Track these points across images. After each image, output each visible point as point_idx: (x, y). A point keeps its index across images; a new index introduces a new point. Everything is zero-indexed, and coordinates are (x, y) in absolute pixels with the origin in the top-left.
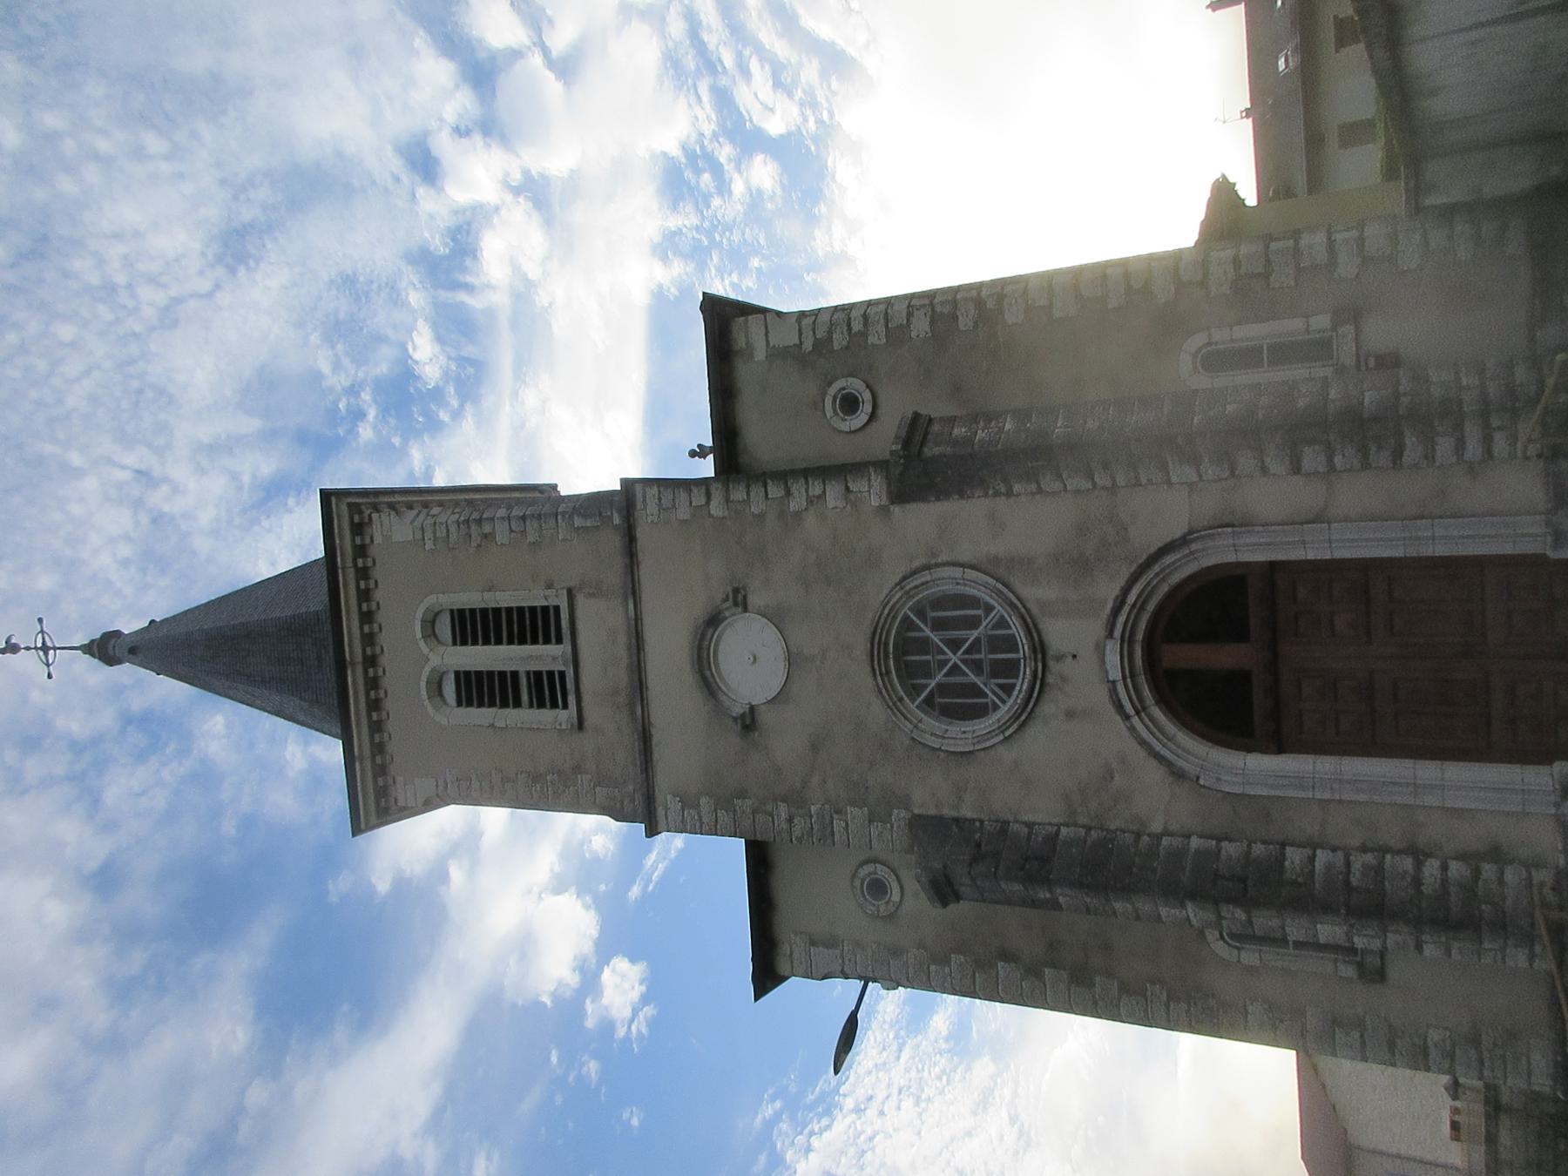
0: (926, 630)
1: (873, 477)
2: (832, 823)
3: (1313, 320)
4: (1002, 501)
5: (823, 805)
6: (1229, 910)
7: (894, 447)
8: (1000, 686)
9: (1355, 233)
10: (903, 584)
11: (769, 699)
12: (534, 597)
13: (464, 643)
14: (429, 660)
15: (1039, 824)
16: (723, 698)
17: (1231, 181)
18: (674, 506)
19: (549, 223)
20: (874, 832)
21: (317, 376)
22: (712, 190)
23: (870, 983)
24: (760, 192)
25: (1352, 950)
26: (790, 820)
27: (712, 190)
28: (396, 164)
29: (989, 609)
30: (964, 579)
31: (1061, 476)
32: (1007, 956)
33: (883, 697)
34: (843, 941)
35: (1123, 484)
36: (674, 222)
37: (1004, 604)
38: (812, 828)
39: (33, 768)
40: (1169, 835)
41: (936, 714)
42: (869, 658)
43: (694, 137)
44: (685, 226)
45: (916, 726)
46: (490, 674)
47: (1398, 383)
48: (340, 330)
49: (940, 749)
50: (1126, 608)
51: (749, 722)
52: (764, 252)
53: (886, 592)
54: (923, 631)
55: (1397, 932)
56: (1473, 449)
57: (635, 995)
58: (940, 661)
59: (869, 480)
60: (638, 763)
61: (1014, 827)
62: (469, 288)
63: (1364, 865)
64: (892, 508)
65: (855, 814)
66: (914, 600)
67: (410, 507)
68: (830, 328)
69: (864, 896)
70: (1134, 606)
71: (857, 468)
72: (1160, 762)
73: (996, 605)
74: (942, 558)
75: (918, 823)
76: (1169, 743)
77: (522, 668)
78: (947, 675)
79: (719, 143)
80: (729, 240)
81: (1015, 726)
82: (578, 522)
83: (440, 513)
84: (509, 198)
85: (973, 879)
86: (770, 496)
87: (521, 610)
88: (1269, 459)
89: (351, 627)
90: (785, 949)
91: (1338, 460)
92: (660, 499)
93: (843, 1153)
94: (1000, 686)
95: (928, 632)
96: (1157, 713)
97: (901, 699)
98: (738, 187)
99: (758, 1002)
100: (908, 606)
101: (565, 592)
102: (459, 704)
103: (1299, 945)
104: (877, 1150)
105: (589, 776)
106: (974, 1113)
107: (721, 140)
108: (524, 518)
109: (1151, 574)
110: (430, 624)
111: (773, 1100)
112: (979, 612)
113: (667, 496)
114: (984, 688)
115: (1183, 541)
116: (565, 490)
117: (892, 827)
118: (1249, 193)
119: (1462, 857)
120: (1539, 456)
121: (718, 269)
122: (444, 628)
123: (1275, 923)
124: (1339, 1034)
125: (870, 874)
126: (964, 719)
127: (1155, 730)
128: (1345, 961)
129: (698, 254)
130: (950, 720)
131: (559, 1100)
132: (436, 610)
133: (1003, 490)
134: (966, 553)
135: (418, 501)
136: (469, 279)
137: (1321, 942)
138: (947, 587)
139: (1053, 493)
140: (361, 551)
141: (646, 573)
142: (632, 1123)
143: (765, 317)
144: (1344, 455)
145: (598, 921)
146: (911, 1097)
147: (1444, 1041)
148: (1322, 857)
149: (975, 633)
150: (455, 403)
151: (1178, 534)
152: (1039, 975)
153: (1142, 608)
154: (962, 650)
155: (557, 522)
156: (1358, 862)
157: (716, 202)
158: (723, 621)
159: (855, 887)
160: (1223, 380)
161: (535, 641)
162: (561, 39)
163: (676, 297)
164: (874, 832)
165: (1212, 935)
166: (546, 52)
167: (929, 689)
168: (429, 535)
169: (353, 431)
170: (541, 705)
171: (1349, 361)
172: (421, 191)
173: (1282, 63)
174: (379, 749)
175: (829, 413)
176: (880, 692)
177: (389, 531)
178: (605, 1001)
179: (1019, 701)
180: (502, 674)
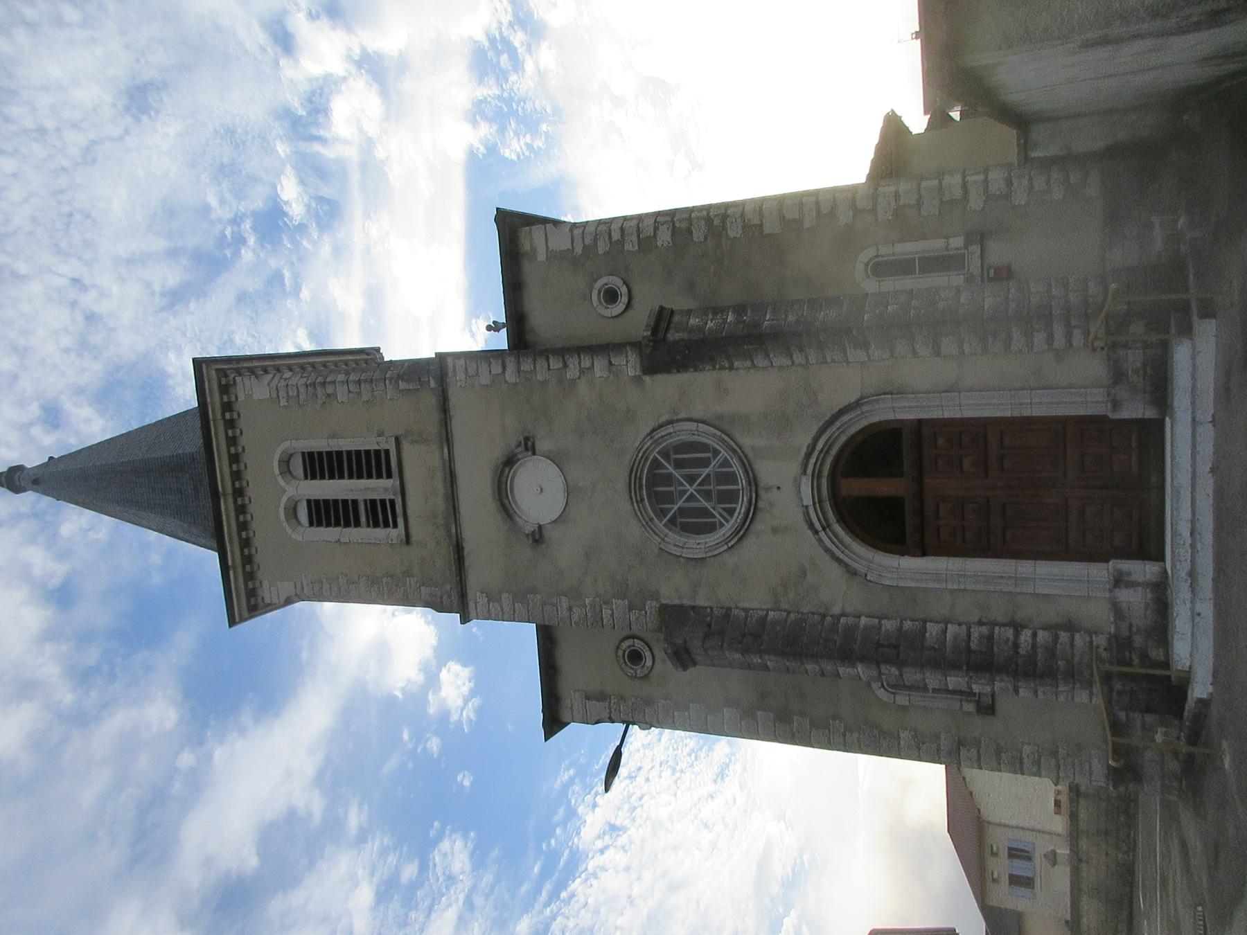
0: (669, 467)
1: (629, 354)
3: (951, 240)
4: (725, 373)
5: (594, 598)
8: (724, 509)
11: (553, 520)
12: (369, 443)
13: (314, 477)
14: (286, 491)
15: (753, 610)
16: (518, 519)
17: (899, 114)
18: (477, 374)
20: (633, 618)
21: (207, 208)
22: (510, 68)
27: (510, 68)
28: (262, 37)
29: (716, 452)
31: (768, 356)
36: (481, 92)
40: (845, 616)
41: (678, 529)
43: (494, 25)
44: (490, 96)
45: (663, 540)
49: (681, 556)
50: (816, 454)
51: (538, 537)
52: (550, 118)
54: (668, 469)
55: (1002, 680)
56: (1059, 341)
57: (465, 690)
58: (680, 491)
59: (627, 356)
60: (454, 568)
61: (735, 612)
62: (322, 140)
64: (644, 377)
65: (619, 605)
69: (625, 663)
70: (821, 451)
73: (722, 450)
74: (683, 415)
75: (664, 610)
76: (846, 550)
78: (687, 501)
79: (514, 30)
80: (523, 108)
81: (736, 539)
82: (402, 385)
84: (353, 69)
86: (551, 368)
91: (966, 347)
93: (619, 809)
94: (724, 509)
96: (838, 528)
97: (651, 520)
98: (529, 66)
99: (547, 742)
100: (657, 451)
102: (311, 524)
104: (645, 807)
106: (715, 781)
109: (834, 428)
110: (286, 463)
111: (568, 769)
112: (710, 455)
115: (857, 404)
117: (646, 613)
118: (917, 122)
119: (1046, 628)
122: (297, 466)
123: (919, 677)
125: (629, 647)
131: (411, 766)
132: (292, 506)
134: (698, 411)
135: (271, 366)
136: (322, 133)
137: (950, 688)
139: (765, 368)
140: (228, 407)
145: (436, 634)
146: (669, 769)
149: (707, 471)
151: (853, 399)
153: (827, 452)
154: (696, 484)
155: (385, 385)
156: (976, 632)
157: (513, 78)
158: (517, 462)
159: (619, 656)
161: (370, 476)
163: (483, 155)
165: (875, 686)
168: (282, 394)
169: (237, 253)
170: (376, 525)
171: (976, 271)
172: (283, 62)
174: (248, 560)
175: (595, 303)
177: (252, 392)
178: (443, 693)
180: (345, 502)
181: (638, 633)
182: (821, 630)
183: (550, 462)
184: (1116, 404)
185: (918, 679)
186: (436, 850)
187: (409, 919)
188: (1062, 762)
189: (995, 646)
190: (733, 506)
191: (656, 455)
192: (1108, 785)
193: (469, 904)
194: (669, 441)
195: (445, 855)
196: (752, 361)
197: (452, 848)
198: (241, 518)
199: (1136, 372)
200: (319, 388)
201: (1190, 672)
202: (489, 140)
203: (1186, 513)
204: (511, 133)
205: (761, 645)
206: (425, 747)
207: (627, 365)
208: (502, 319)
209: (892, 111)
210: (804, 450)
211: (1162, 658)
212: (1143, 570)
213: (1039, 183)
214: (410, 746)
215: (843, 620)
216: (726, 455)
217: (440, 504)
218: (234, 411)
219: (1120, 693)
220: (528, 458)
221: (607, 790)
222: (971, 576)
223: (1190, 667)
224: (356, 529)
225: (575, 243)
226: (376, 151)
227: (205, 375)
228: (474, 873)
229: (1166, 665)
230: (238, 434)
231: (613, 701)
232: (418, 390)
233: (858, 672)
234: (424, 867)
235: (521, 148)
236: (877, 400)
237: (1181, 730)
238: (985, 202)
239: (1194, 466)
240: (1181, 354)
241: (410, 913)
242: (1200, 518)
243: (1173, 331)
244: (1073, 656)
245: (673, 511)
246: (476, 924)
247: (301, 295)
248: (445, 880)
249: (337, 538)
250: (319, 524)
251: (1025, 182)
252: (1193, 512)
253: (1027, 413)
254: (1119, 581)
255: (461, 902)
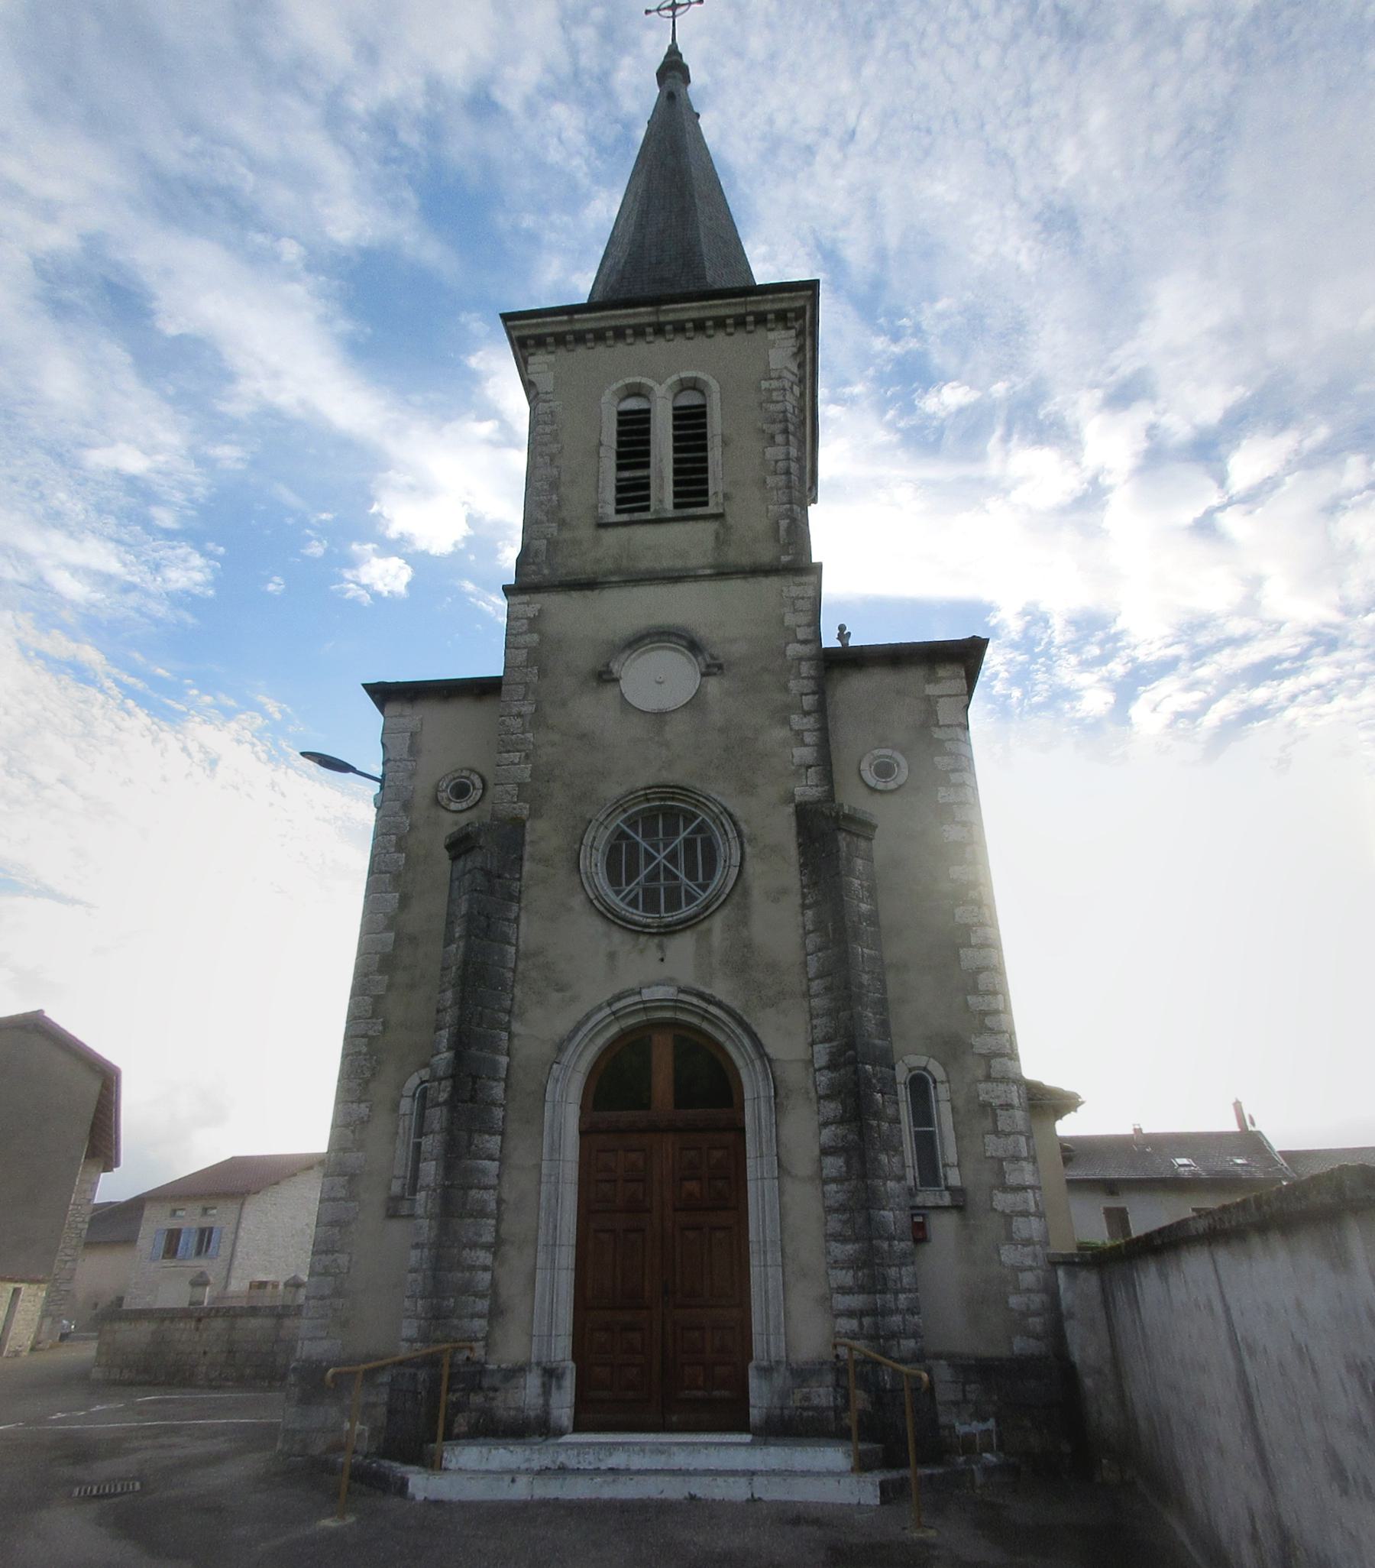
1: (819, 789)
2: (518, 751)
3: (956, 1171)
4: (798, 900)
6: (446, 1087)
7: (846, 808)
8: (637, 895)
9: (1033, 1209)
10: (725, 814)
11: (626, 695)
12: (716, 484)
13: (676, 417)
14: (660, 385)
15: (518, 928)
16: (626, 655)
17: (1079, 1109)
19: (1063, 511)
20: (509, 787)
21: (933, 298)
22: (1084, 657)
23: (379, 784)
24: (1079, 698)
25: (414, 1190)
26: (519, 715)
28: (1126, 370)
30: (729, 867)
31: (820, 950)
32: (404, 901)
33: (627, 796)
34: (415, 761)
35: (813, 1004)
36: (1057, 623)
37: (707, 901)
38: (513, 734)
39: (586, 35)
40: (509, 1038)
41: (613, 841)
42: (660, 784)
43: (1133, 640)
45: (602, 823)
46: (647, 442)
47: (901, 1240)
48: (974, 322)
49: (581, 843)
50: (704, 1005)
51: (605, 677)
52: (1026, 701)
53: (719, 799)
54: (684, 830)
55: (430, 1228)
56: (843, 1302)
57: (380, 586)
58: (658, 845)
59: (817, 786)
60: (568, 578)
61: (515, 908)
62: (1006, 439)
63: (485, 1201)
64: (793, 805)
65: (525, 772)
66: (711, 824)
67: (801, 366)
68: (952, 754)
69: (454, 779)
70: (706, 1011)
71: (828, 776)
72: (571, 1032)
73: (707, 894)
74: (748, 849)
75: (517, 826)
77: (652, 472)
79: (1127, 662)
80: (1038, 670)
81: (602, 909)
82: (784, 523)
83: (794, 395)
84: (1088, 474)
85: (470, 871)
86: (804, 697)
87: (705, 470)
88: (833, 1129)
89: (691, 311)
90: (407, 710)
91: (833, 1187)
92: (803, 598)
94: (637, 895)
95: (683, 835)
96: (614, 1029)
97: (625, 811)
98: (1086, 679)
101: (721, 511)
102: (620, 413)
103: (418, 1147)
105: (555, 534)
107: (1130, 665)
108: (788, 472)
109: (733, 1025)
112: (701, 880)
113: (805, 605)
114: (635, 882)
115: (763, 1054)
116: (812, 510)
117: (515, 803)
118: (1067, 1127)
119: (494, 1284)
120: (837, 1356)
121: (1011, 661)
122: (689, 399)
123: (436, 1126)
124: (343, 1180)
125: (473, 785)
126: (608, 863)
127: (600, 1027)
128: (404, 1185)
129: (1027, 643)
130: (607, 853)
133: (807, 901)
134: (753, 868)
136: (1015, 437)
137: (421, 1165)
138: (722, 850)
139: (804, 945)
140: (761, 319)
141: (736, 585)
142: (271, 585)
143: (964, 695)
144: (837, 1192)
147: (338, 1267)
148: (492, 1166)
149: (682, 876)
150: (902, 424)
151: (769, 1050)
152: (388, 928)
153: (704, 1018)
156: (490, 1196)
157: (1073, 659)
160: (903, 1093)
161: (676, 483)
162: (1231, 521)
163: (988, 622)
164: (509, 787)
165: (425, 1073)
166: (1221, 508)
167: (632, 834)
168: (775, 384)
169: (880, 331)
170: (619, 489)
171: (919, 1200)
172: (1099, 394)
173: (1184, 1161)
174: (580, 338)
176: (632, 793)
177: (779, 344)
178: (374, 560)
179: (623, 912)
180: (647, 453)
181: (489, 794)
182: (493, 1009)
183: (693, 693)
184: (766, 1372)
185: (433, 1126)
186: (190, 550)
187: (105, 515)
188: (328, 1302)
189: (472, 1220)
190: (641, 906)
191: (701, 818)
192: (297, 1360)
193: (128, 588)
194: (717, 833)
195: (185, 560)
196: (812, 932)
197: (193, 568)
198: (629, 332)
199: (807, 1398)
200: (781, 426)
201: (440, 1469)
202: (1003, 630)
203: (638, 1462)
204: (1011, 656)
205: (476, 936)
206: (310, 539)
207: (807, 785)
208: (853, 642)
209: (1083, 1103)
210: (708, 991)
211: (456, 1431)
212: (563, 1405)
213: (1028, 1279)
214: (313, 521)
215: (504, 1035)
216: (701, 899)
217: (644, 564)
218: (755, 326)
219: (414, 1377)
220: (697, 667)
221: (303, 754)
222: (557, 1189)
223: (446, 1469)
224: (614, 465)
225: (946, 729)
226: (994, 499)
227: (799, 293)
228: (164, 594)
229: (449, 1436)
230: (688, 334)
231: (409, 763)
232: (778, 541)
233: (443, 1053)
234: (169, 534)
235: (993, 666)
236: (768, 1079)
237: (366, 1457)
238: (1003, 1212)
239: (695, 1473)
240: (834, 1457)
241: (113, 518)
242: (633, 1482)
243: (862, 1447)
244: (460, 1318)
245: (635, 836)
246: (103, 596)
247: (832, 406)
248: (154, 559)
249: (605, 443)
250: (620, 423)
251: (1029, 1262)
252: (639, 1472)
253: (754, 1261)
254: (551, 1374)
255: (129, 578)
